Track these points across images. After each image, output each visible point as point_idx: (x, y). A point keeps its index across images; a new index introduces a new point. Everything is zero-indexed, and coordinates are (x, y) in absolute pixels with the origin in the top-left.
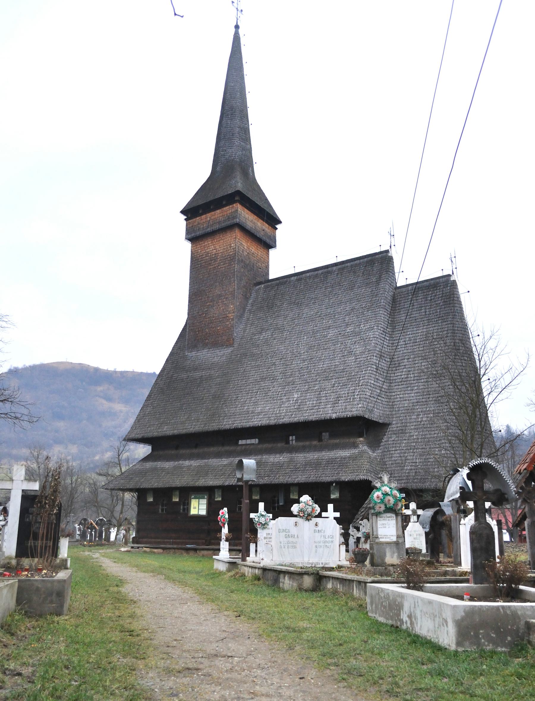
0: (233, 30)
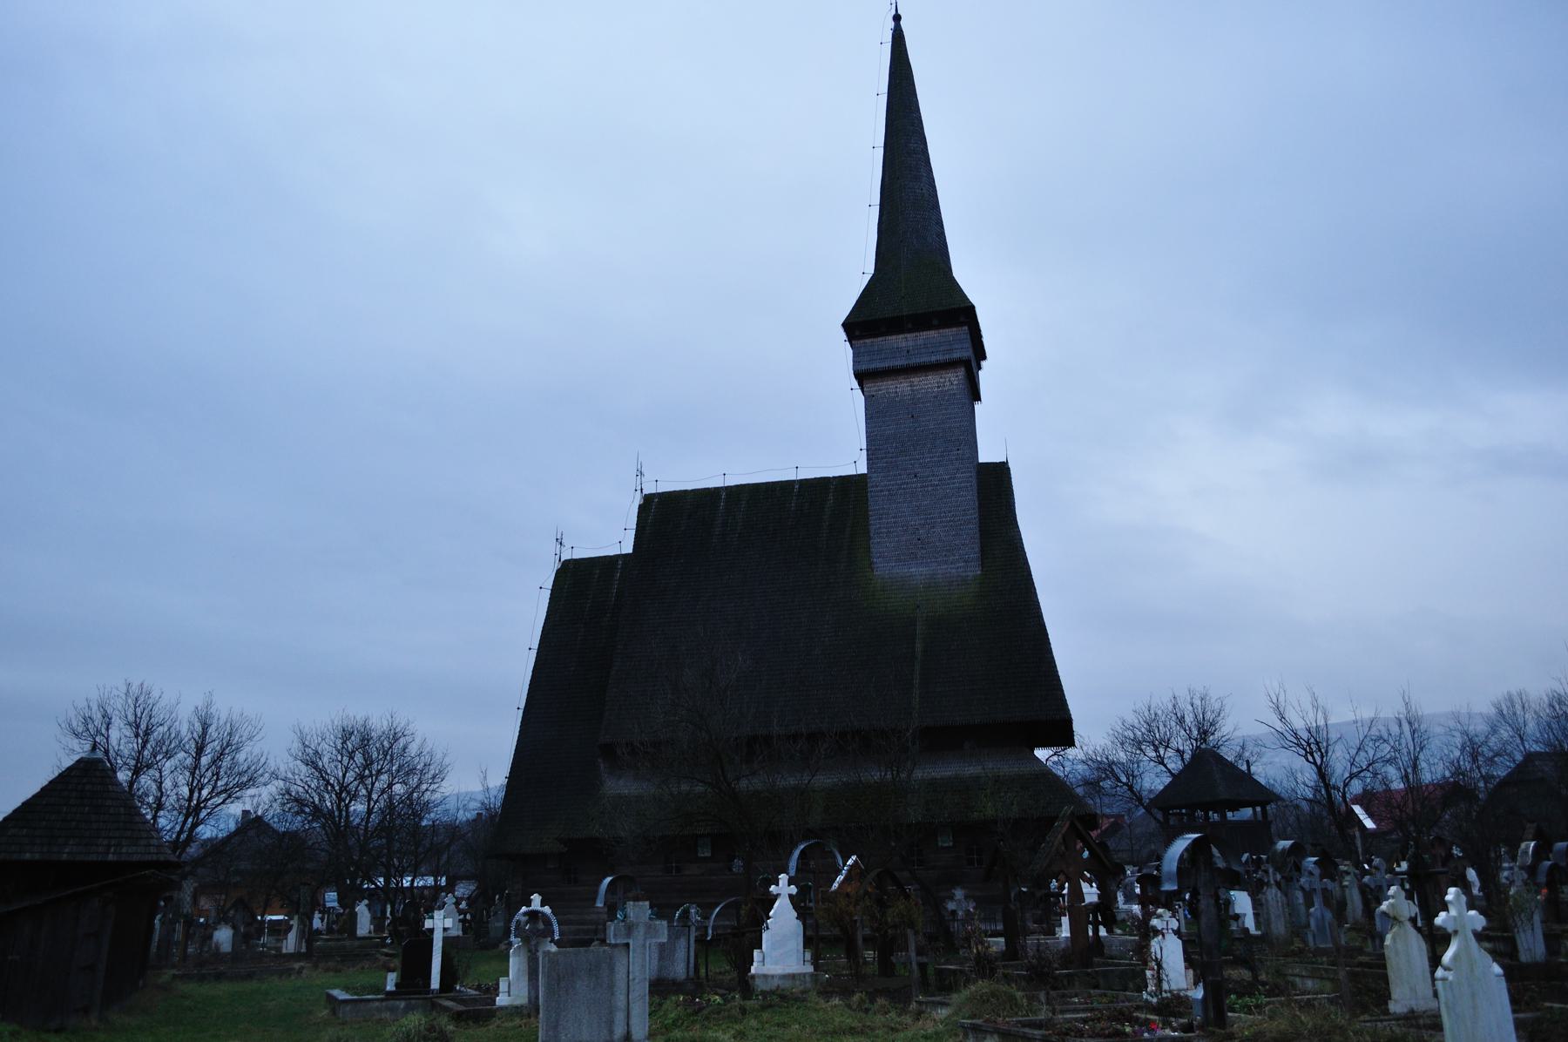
0: (892, 24)
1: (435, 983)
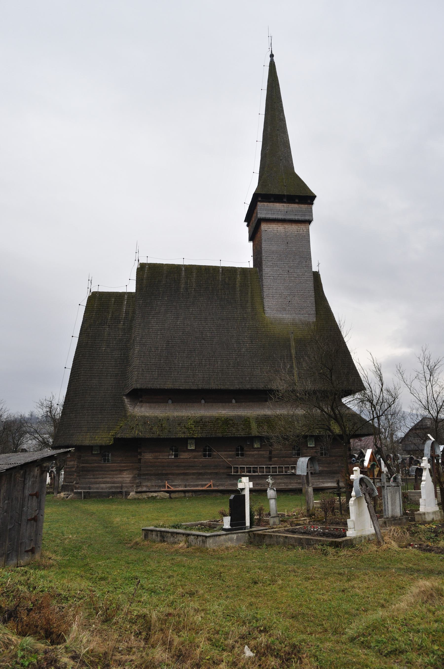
0: (269, 59)
1: (248, 523)
